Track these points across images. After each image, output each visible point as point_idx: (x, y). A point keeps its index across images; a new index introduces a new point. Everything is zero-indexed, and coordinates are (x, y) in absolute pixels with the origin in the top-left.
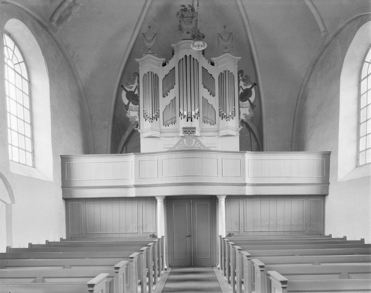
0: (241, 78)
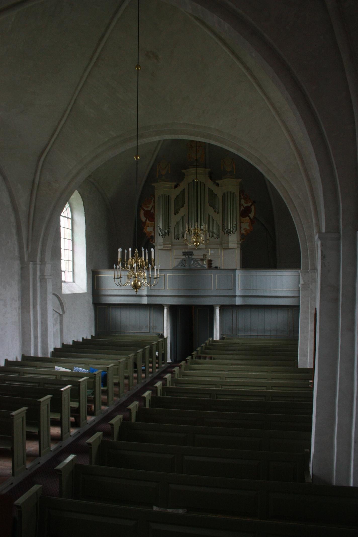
0: (242, 197)
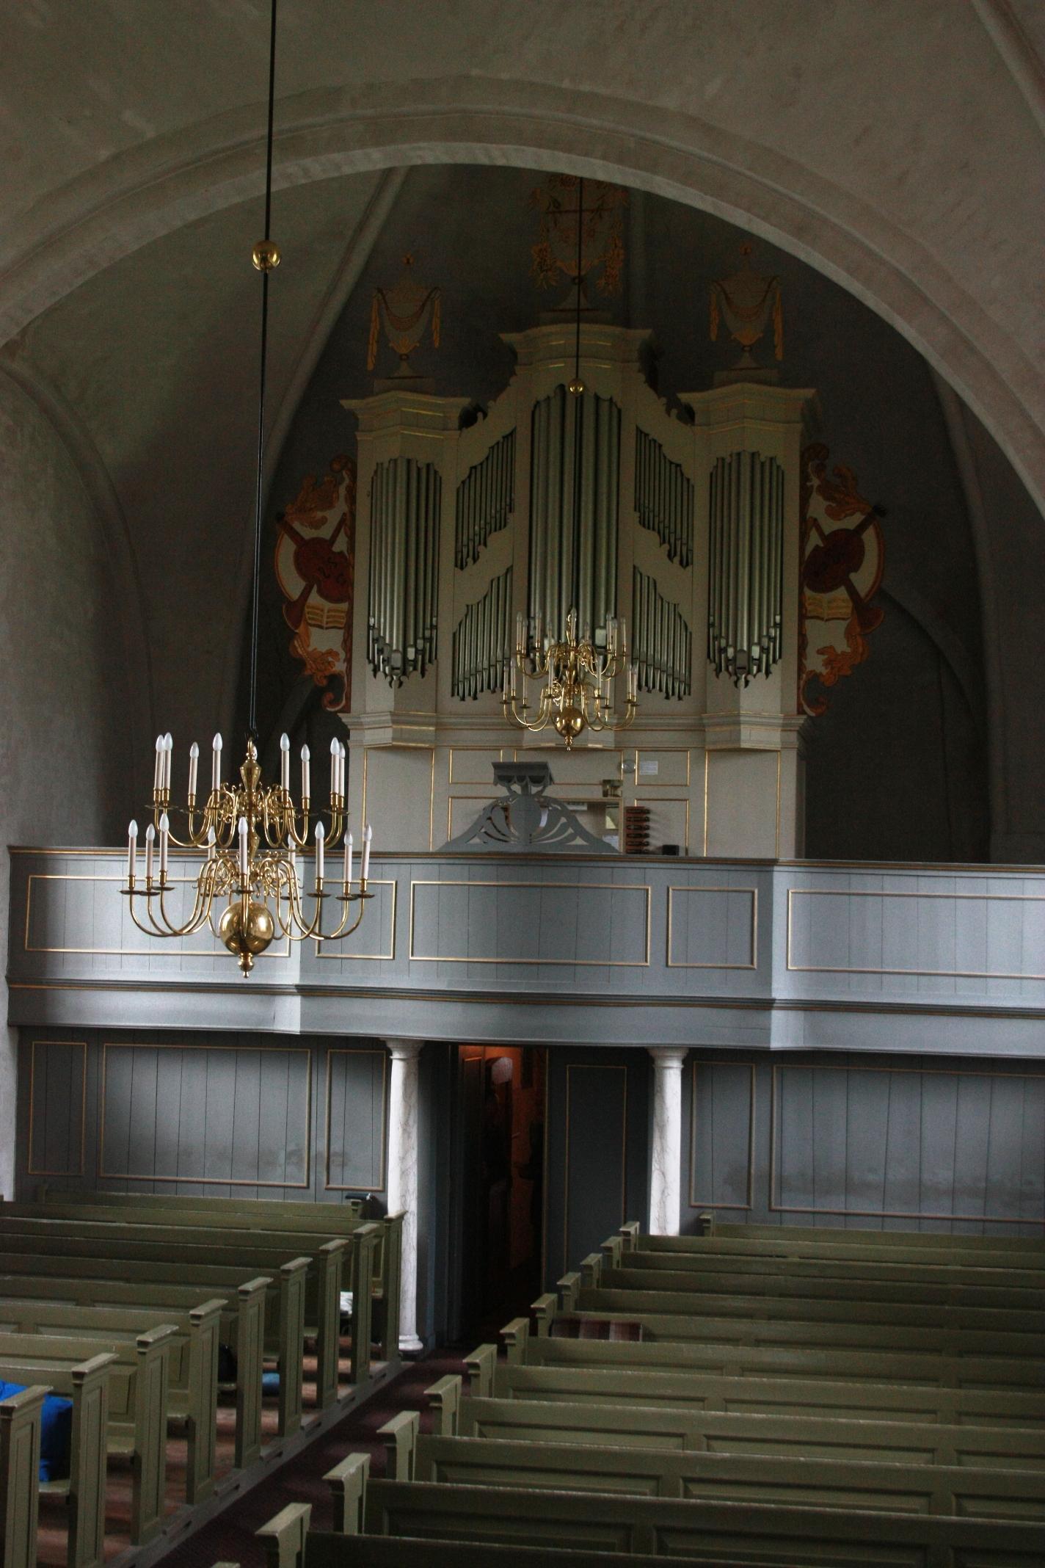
0: (815, 482)
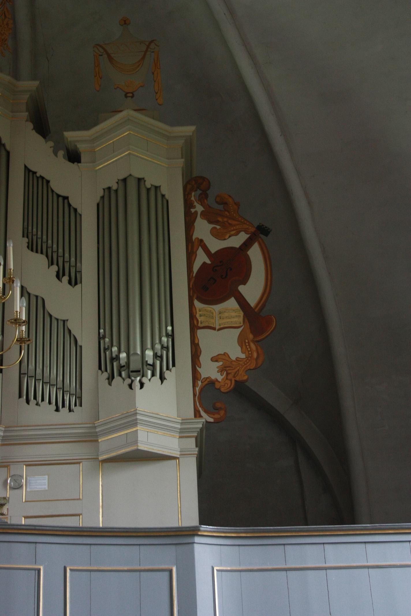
0: (199, 208)
